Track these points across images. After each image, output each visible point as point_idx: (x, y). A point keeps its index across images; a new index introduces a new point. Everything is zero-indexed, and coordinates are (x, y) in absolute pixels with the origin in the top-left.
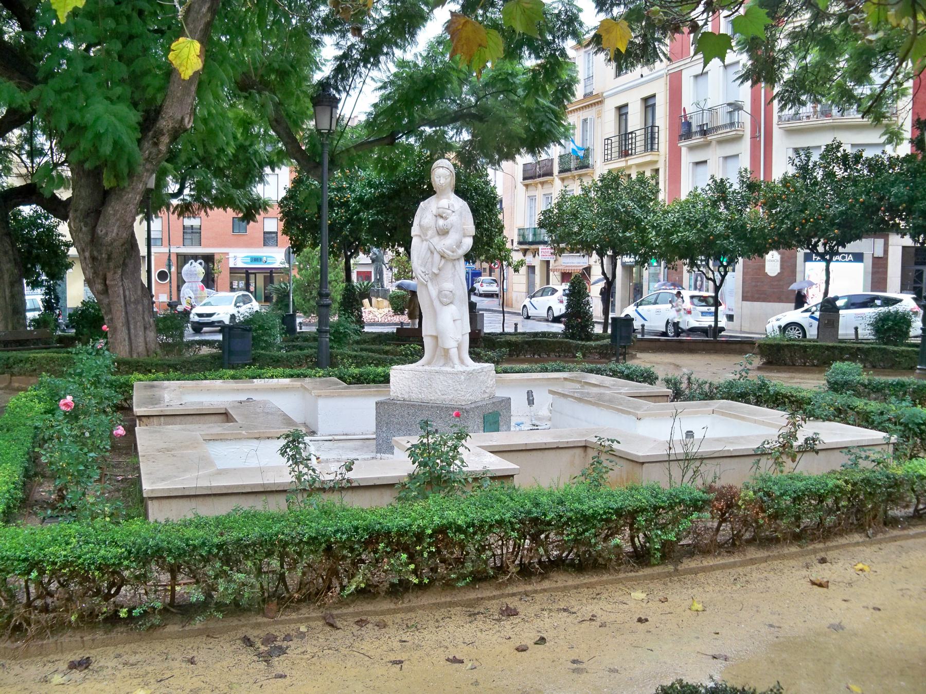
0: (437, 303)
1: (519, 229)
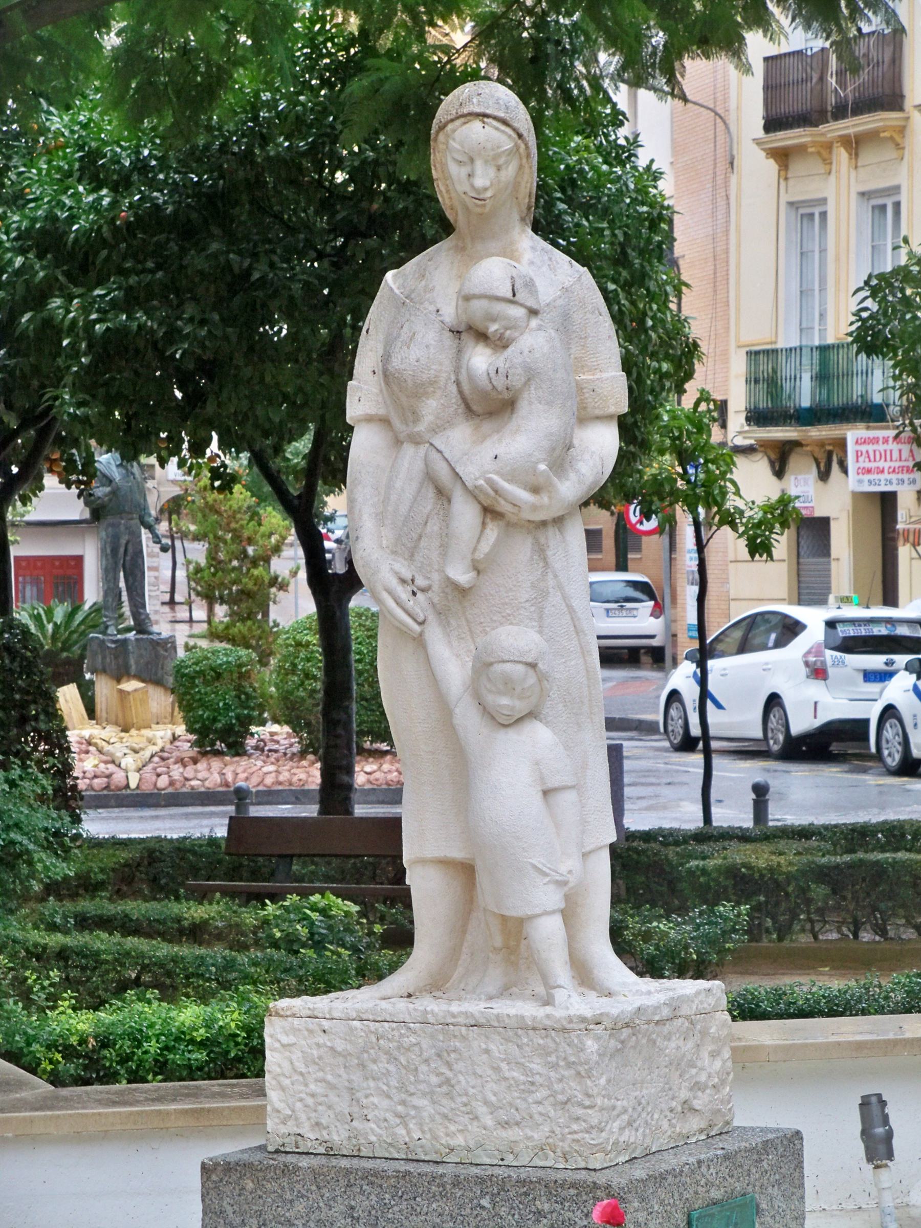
0: (468, 718)
1: (753, 355)
